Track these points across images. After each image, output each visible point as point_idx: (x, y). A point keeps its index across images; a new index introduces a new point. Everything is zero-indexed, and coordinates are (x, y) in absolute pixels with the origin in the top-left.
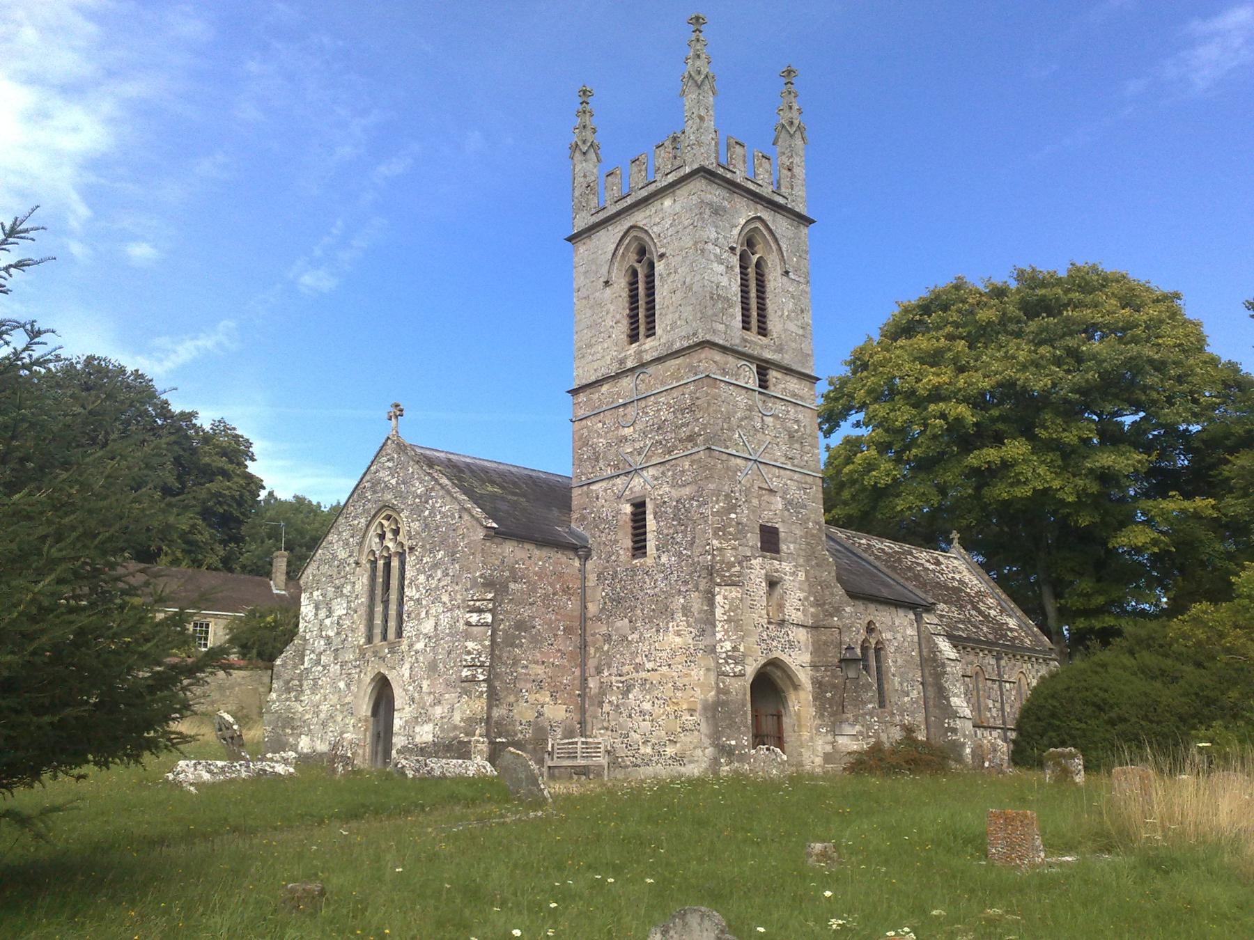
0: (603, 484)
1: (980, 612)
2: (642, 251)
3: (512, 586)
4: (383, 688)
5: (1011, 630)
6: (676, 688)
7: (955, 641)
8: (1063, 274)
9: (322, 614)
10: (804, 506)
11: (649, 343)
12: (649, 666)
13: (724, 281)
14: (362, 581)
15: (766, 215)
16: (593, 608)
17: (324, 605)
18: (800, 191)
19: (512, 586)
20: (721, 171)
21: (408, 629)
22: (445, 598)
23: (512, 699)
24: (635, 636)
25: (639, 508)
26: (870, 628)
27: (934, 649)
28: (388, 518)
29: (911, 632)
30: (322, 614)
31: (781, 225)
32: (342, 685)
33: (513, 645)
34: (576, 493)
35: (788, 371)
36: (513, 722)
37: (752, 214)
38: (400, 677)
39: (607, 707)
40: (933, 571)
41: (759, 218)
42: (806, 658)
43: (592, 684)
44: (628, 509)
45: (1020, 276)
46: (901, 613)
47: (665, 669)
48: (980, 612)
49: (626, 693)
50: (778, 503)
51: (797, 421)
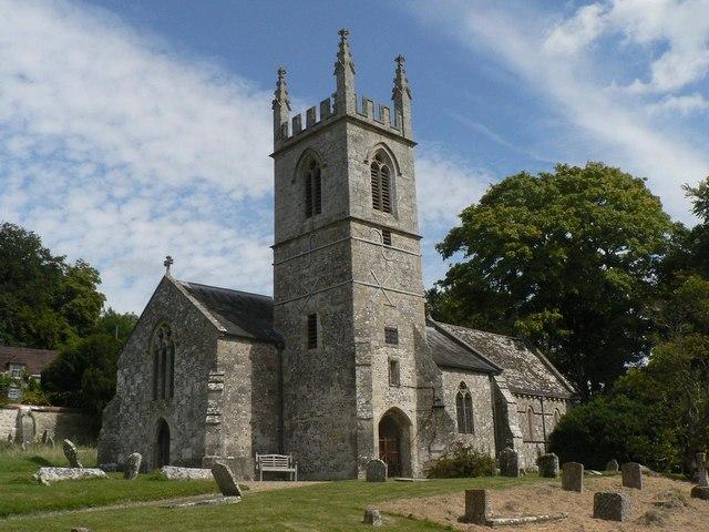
1: (533, 373)
2: (314, 163)
3: (236, 366)
5: (551, 383)
6: (334, 426)
7: (516, 393)
8: (583, 167)
9: (129, 382)
10: (413, 315)
11: (317, 218)
12: (319, 413)
13: (362, 181)
14: (150, 363)
16: (286, 379)
18: (408, 127)
19: (236, 366)
20: (358, 117)
21: (177, 391)
22: (197, 375)
23: (237, 434)
24: (311, 395)
25: (313, 318)
26: (463, 386)
28: (164, 325)
30: (129, 382)
31: (395, 146)
32: (140, 425)
33: (237, 401)
34: (275, 309)
35: (402, 233)
38: (173, 420)
39: (295, 438)
40: (506, 350)
41: (383, 143)
42: (414, 406)
43: (286, 424)
44: (305, 318)
45: (559, 168)
47: (328, 415)
48: (533, 373)
49: (306, 429)
51: (408, 263)
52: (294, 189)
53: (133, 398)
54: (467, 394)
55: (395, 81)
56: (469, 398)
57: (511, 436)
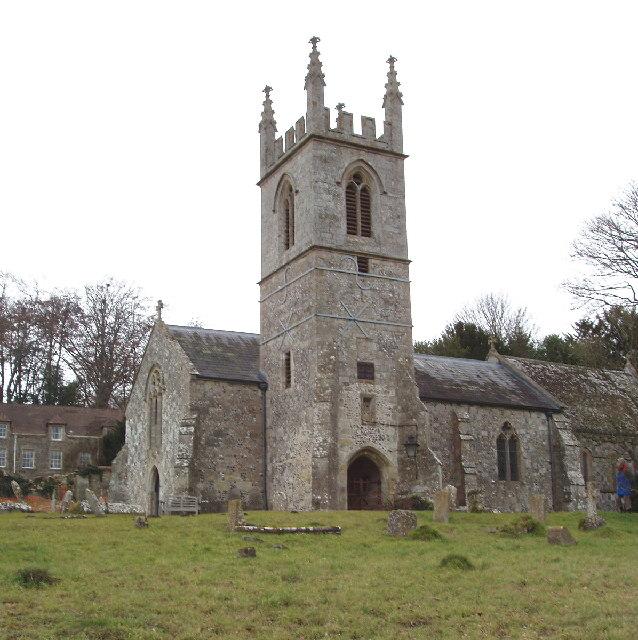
0: (273, 342)
3: (211, 410)
4: (156, 471)
7: (577, 432)
15: (364, 155)
17: (134, 428)
19: (211, 410)
26: (506, 426)
27: (559, 439)
29: (543, 428)
33: (213, 445)
34: (262, 348)
36: (214, 491)
37: (355, 158)
39: (275, 482)
41: (362, 160)
42: (395, 446)
44: (283, 357)
46: (534, 415)
50: (374, 347)
52: (276, 217)
53: (136, 448)
54: (512, 437)
55: (265, 103)
56: (514, 441)
57: (568, 482)
